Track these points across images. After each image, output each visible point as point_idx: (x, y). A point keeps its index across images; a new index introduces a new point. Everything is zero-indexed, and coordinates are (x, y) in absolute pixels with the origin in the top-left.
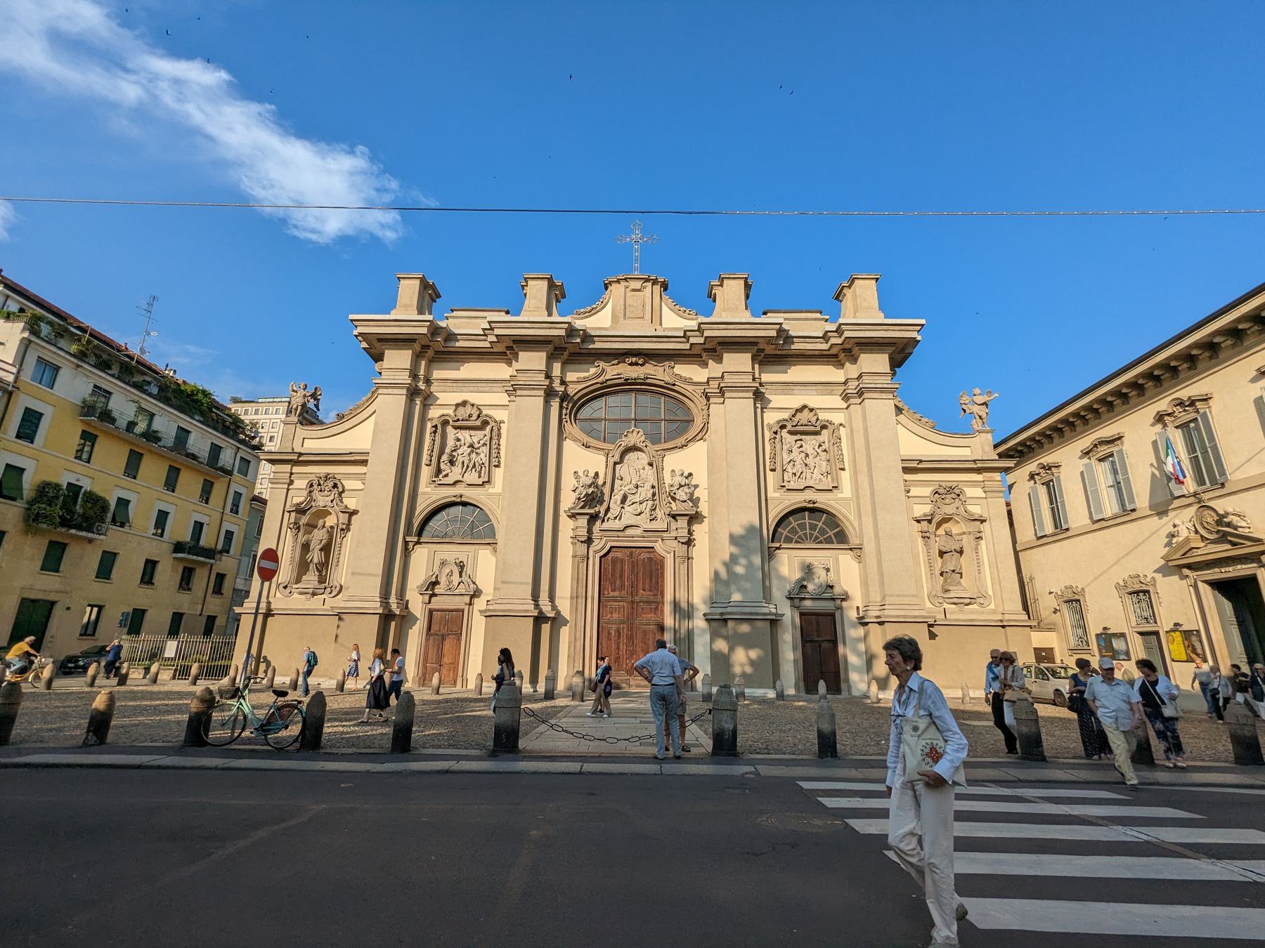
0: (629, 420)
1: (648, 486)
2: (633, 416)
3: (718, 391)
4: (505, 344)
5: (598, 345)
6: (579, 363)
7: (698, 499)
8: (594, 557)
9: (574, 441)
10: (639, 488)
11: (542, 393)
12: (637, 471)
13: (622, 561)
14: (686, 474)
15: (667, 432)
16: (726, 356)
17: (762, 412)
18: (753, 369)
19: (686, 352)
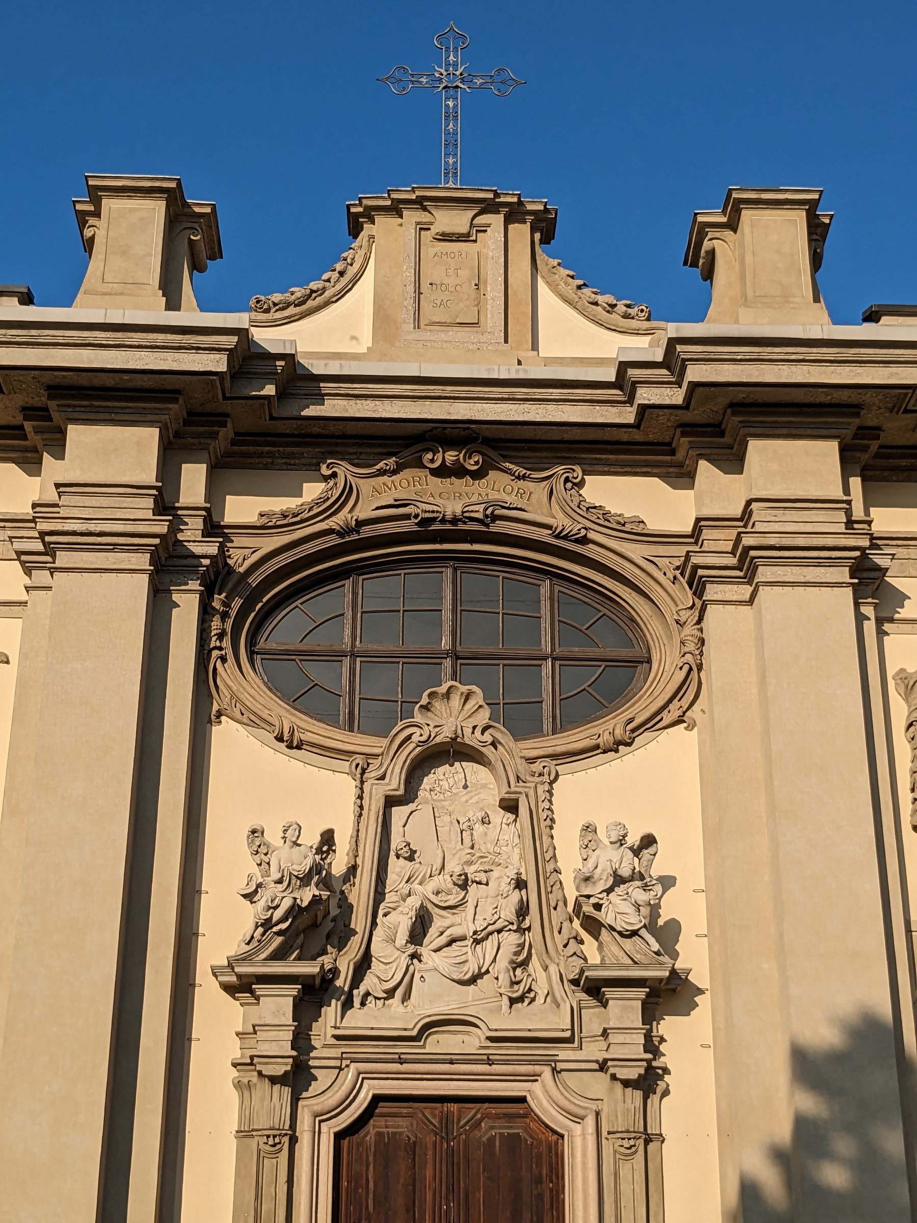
0: (435, 658)
1: (501, 880)
2: (445, 643)
3: (733, 561)
4: (20, 400)
5: (333, 408)
6: (266, 467)
7: (674, 927)
8: (316, 1134)
9: (251, 724)
10: (473, 888)
11: (143, 560)
12: (465, 830)
13: (413, 1148)
14: (633, 839)
15: (563, 700)
16: (755, 447)
17: (881, 633)
18: (846, 490)
19: (624, 436)
